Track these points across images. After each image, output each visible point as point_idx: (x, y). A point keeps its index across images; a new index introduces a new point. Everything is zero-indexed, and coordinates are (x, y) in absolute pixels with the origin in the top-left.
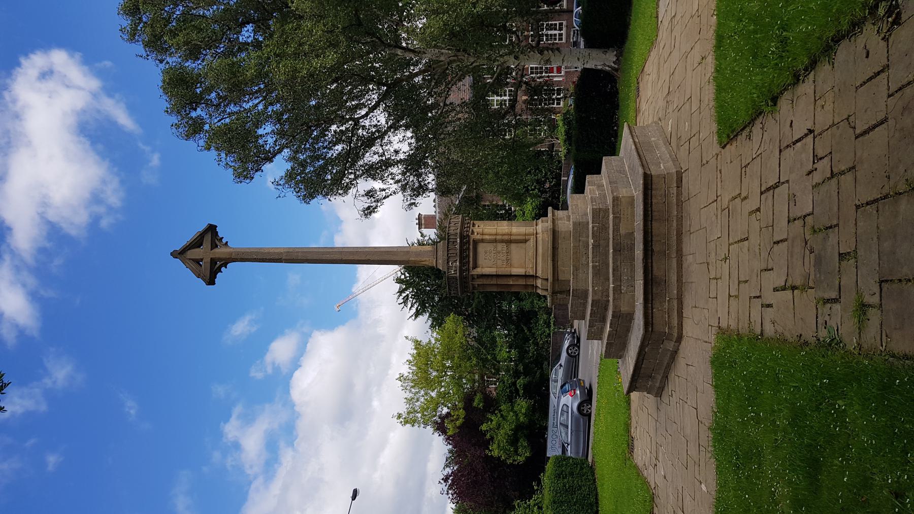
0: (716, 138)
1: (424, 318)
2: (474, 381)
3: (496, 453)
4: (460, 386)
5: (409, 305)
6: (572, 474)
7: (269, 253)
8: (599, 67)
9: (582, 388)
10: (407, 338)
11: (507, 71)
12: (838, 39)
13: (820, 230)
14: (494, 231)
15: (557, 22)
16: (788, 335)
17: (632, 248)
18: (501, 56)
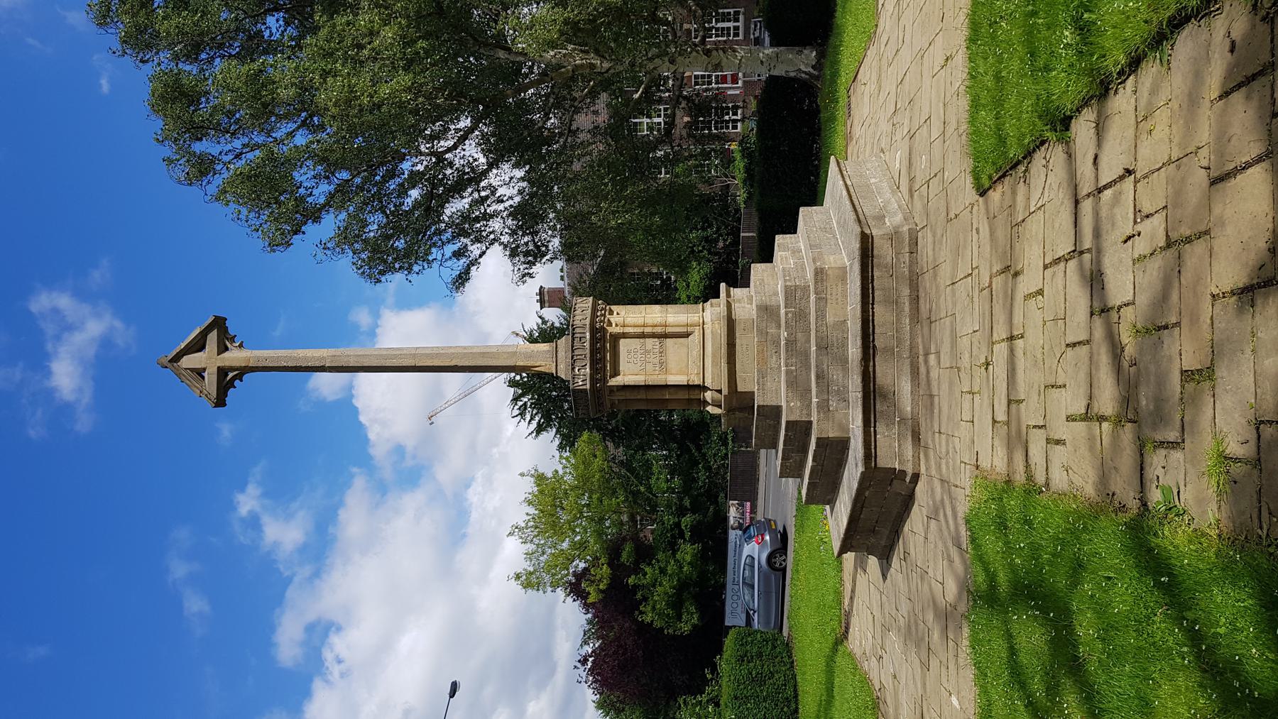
1: (550, 438)
2: (622, 524)
4: (600, 534)
5: (528, 417)
8: (792, 74)
9: (773, 532)
10: (522, 475)
14: (641, 321)
15: (732, 11)
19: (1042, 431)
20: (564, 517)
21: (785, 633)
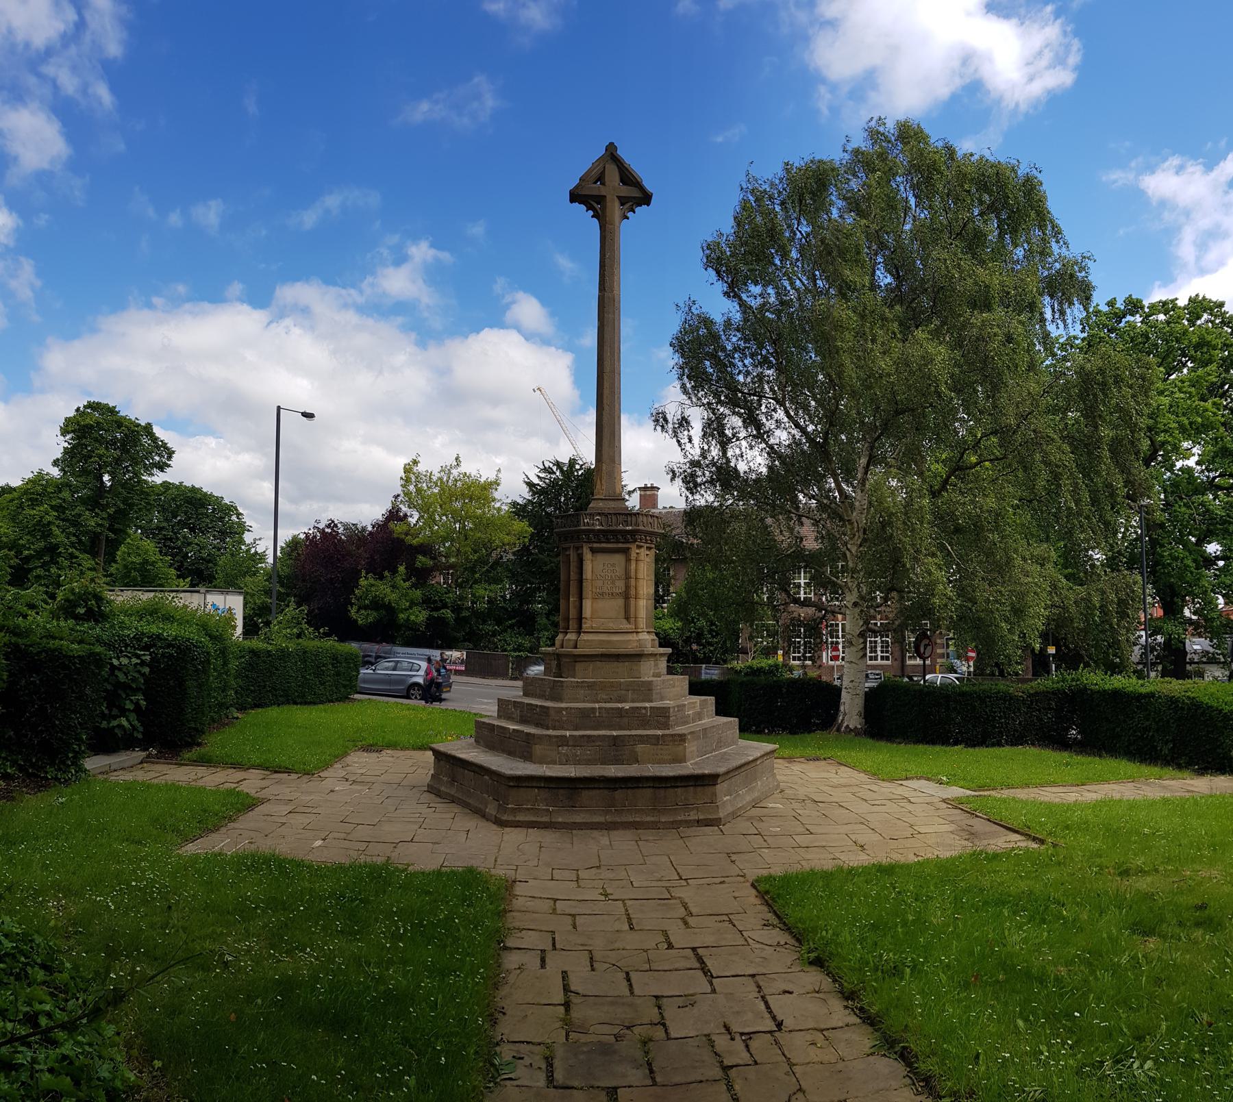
0: (765, 873)
1: (521, 494)
3: (363, 582)
5: (542, 475)
6: (338, 674)
7: (613, 274)
8: (842, 708)
12: (905, 1056)
13: (647, 1053)
14: (640, 575)
16: (504, 991)
17: (617, 761)
18: (858, 586)
19: (551, 947)
20: (458, 505)
21: (357, 696)
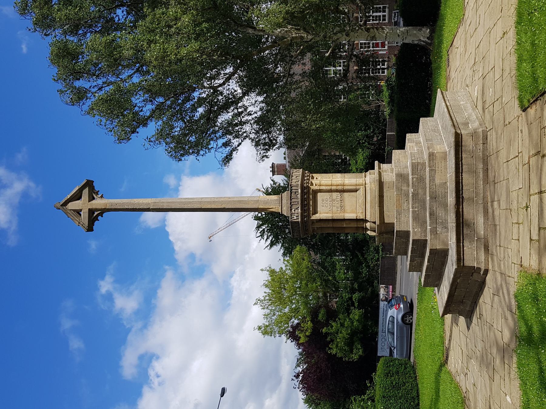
1: (278, 249)
2: (319, 298)
5: (265, 237)
8: (416, 42)
9: (405, 303)
11: (339, 46)
14: (329, 183)
15: (381, 6)
21: (412, 360)
